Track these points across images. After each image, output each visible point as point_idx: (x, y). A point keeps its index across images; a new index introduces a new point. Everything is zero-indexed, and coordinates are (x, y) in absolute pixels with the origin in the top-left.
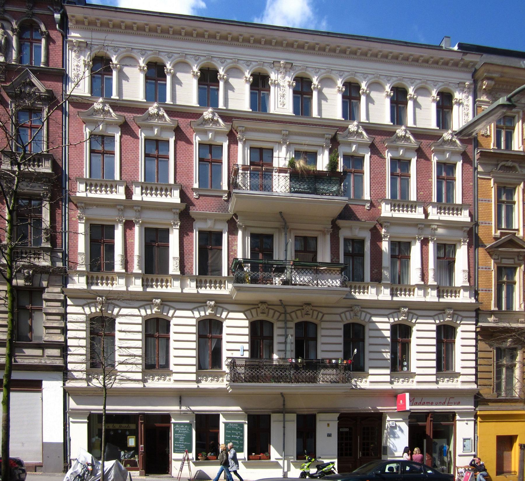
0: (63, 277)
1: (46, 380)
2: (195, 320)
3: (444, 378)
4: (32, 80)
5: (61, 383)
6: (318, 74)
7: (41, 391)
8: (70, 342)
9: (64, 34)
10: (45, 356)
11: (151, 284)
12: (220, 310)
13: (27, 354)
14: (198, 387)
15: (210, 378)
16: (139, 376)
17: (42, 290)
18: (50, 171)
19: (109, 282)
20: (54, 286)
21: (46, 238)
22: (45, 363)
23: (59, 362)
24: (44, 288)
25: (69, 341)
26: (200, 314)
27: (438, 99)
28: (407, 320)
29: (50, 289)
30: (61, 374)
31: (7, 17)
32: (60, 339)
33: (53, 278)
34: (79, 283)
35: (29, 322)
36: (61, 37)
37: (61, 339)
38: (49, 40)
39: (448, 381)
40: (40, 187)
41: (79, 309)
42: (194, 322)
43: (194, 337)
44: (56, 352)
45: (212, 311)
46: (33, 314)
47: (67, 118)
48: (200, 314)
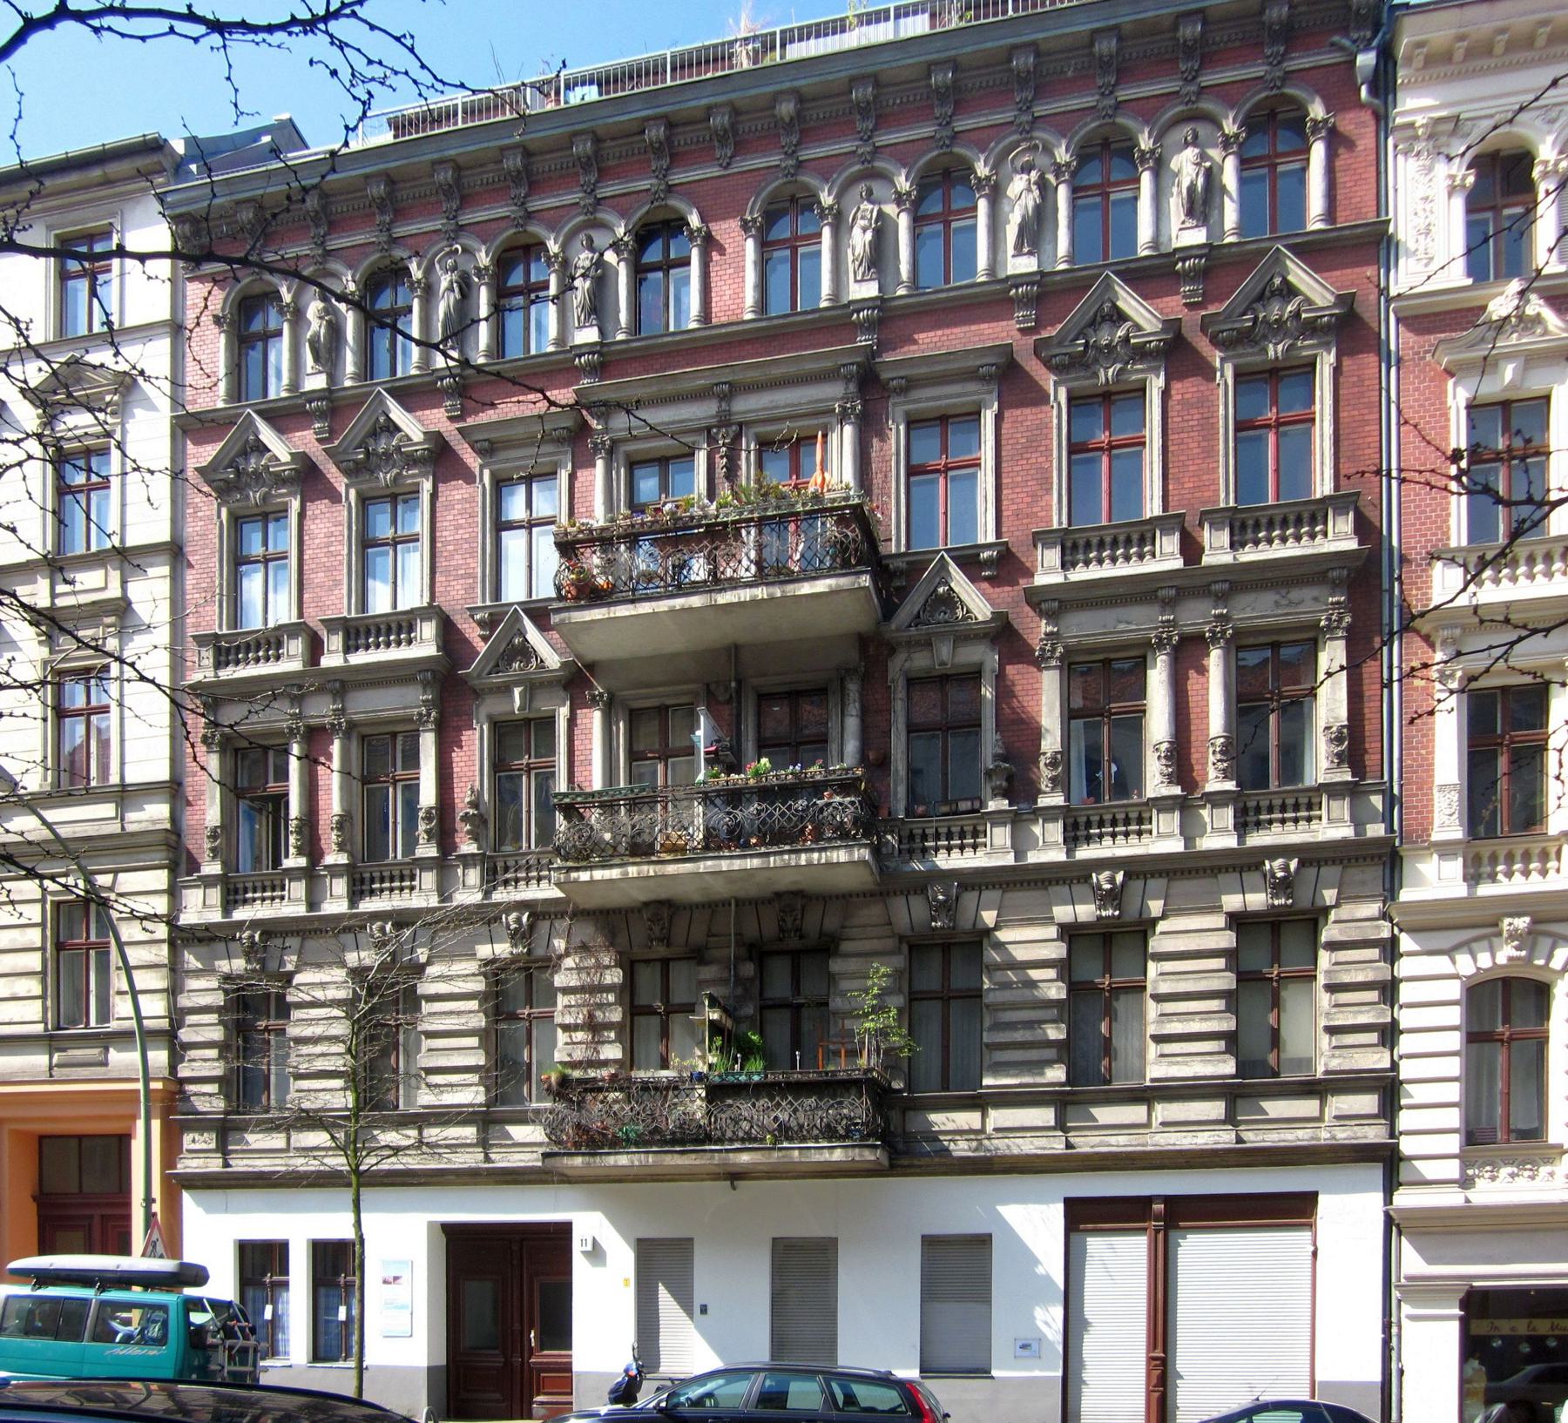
0: (1381, 862)
1: (1330, 1192)
2: (1457, 982)
3: (1495, 1166)
4: (1119, 304)
5: (1378, 1197)
6: (1558, 124)
7: (1311, 1226)
8: (1407, 1070)
9: (1382, 110)
10: (1155, 1123)
11: (1488, 869)
12: (1545, 943)
13: (1272, 1115)
14: (1467, 1201)
15: (1509, 1169)
16: (1452, 1169)
17: (1145, 927)
18: (1352, 545)
19: (1532, 866)
20: (1357, 898)
21: (427, 832)
22: (1334, 1138)
23: (1374, 1134)
24: (988, 932)
25: (1403, 1064)
26: (1475, 960)
27: (1471, 180)
28: (1529, 960)
29: (1346, 911)
30: (1376, 1172)
31: (1207, 105)
32: (1379, 1060)
33: (1355, 874)
34: (1435, 880)
35: (1104, 1028)
36: (1372, 122)
37: (1378, 1060)
38: (1336, 142)
39: (1513, 1175)
40: (1316, 599)
41: (1441, 964)
42: (1454, 990)
43: (1454, 1041)
44: (1367, 1103)
45: (1517, 948)
46: (1283, 994)
47: (1393, 370)
48: (1475, 960)
